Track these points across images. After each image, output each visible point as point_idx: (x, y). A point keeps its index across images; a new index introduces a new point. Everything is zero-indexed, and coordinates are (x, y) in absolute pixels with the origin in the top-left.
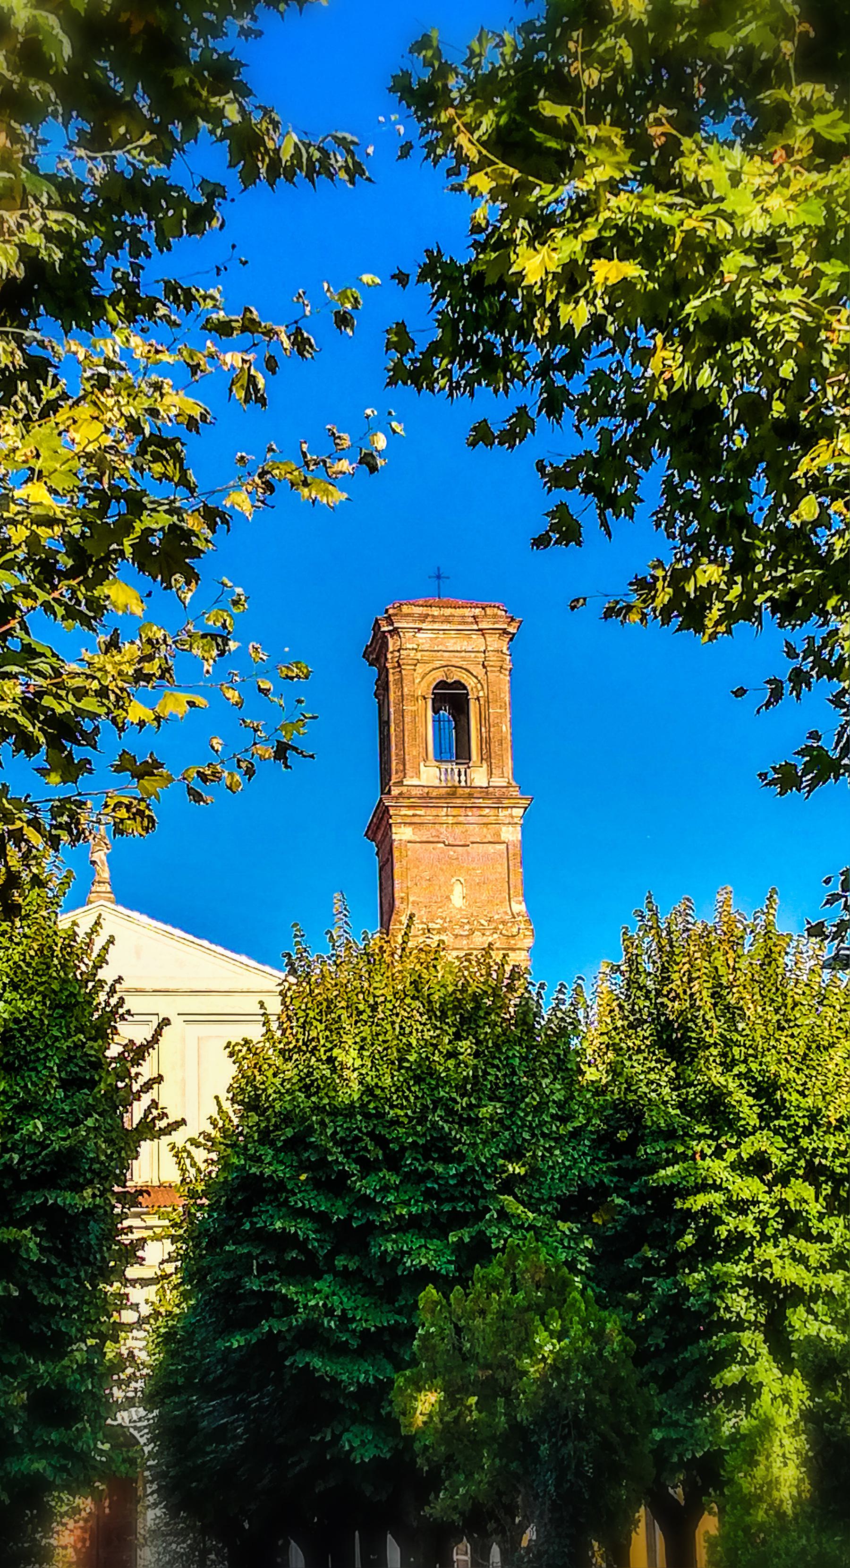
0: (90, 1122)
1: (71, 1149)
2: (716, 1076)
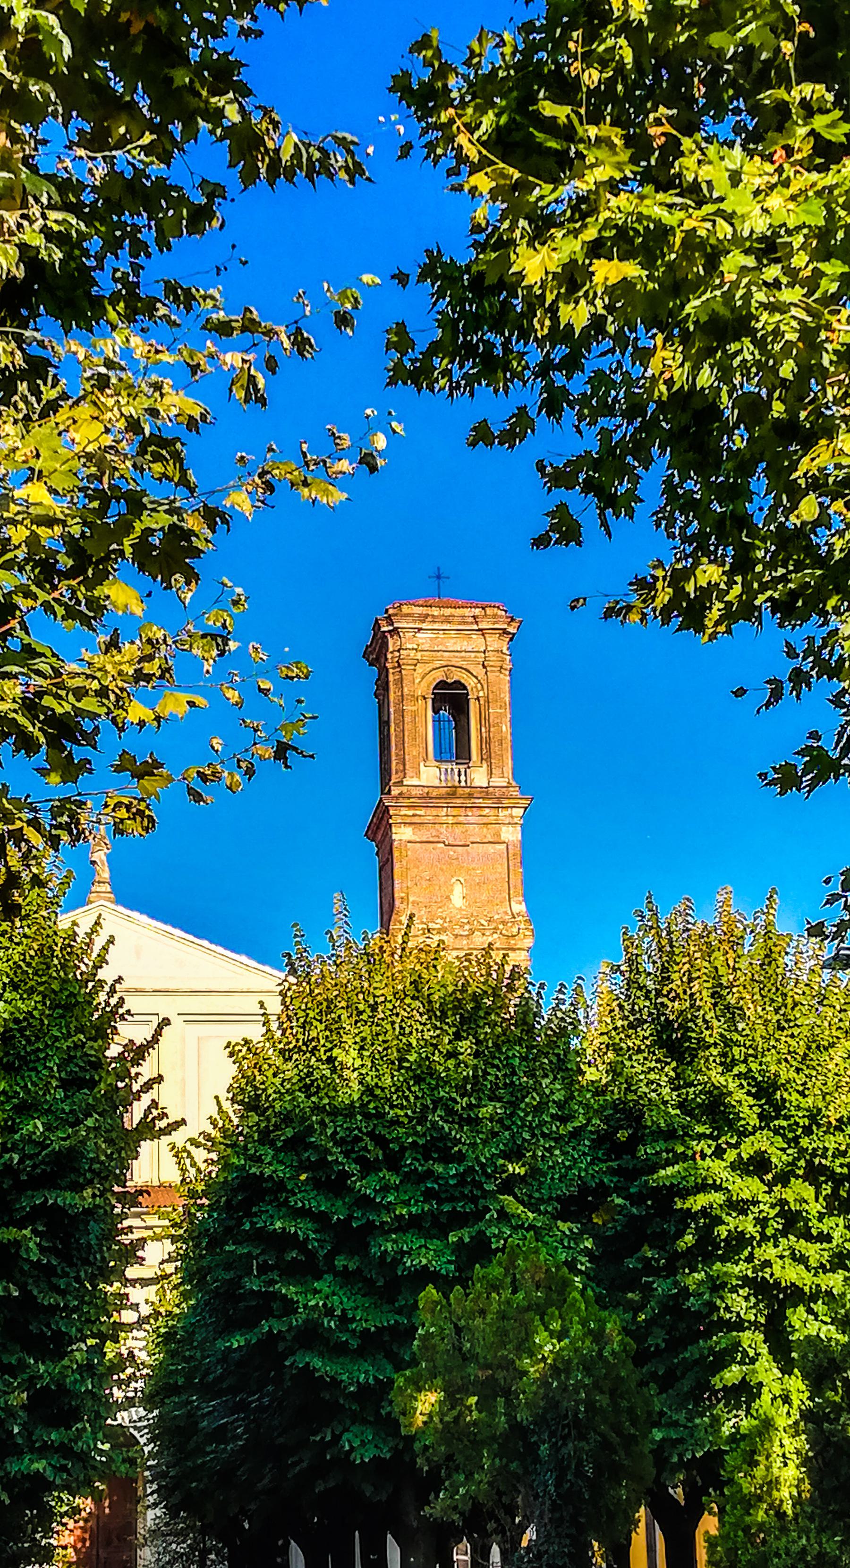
0: (90, 1122)
1: (71, 1149)
2: (716, 1076)
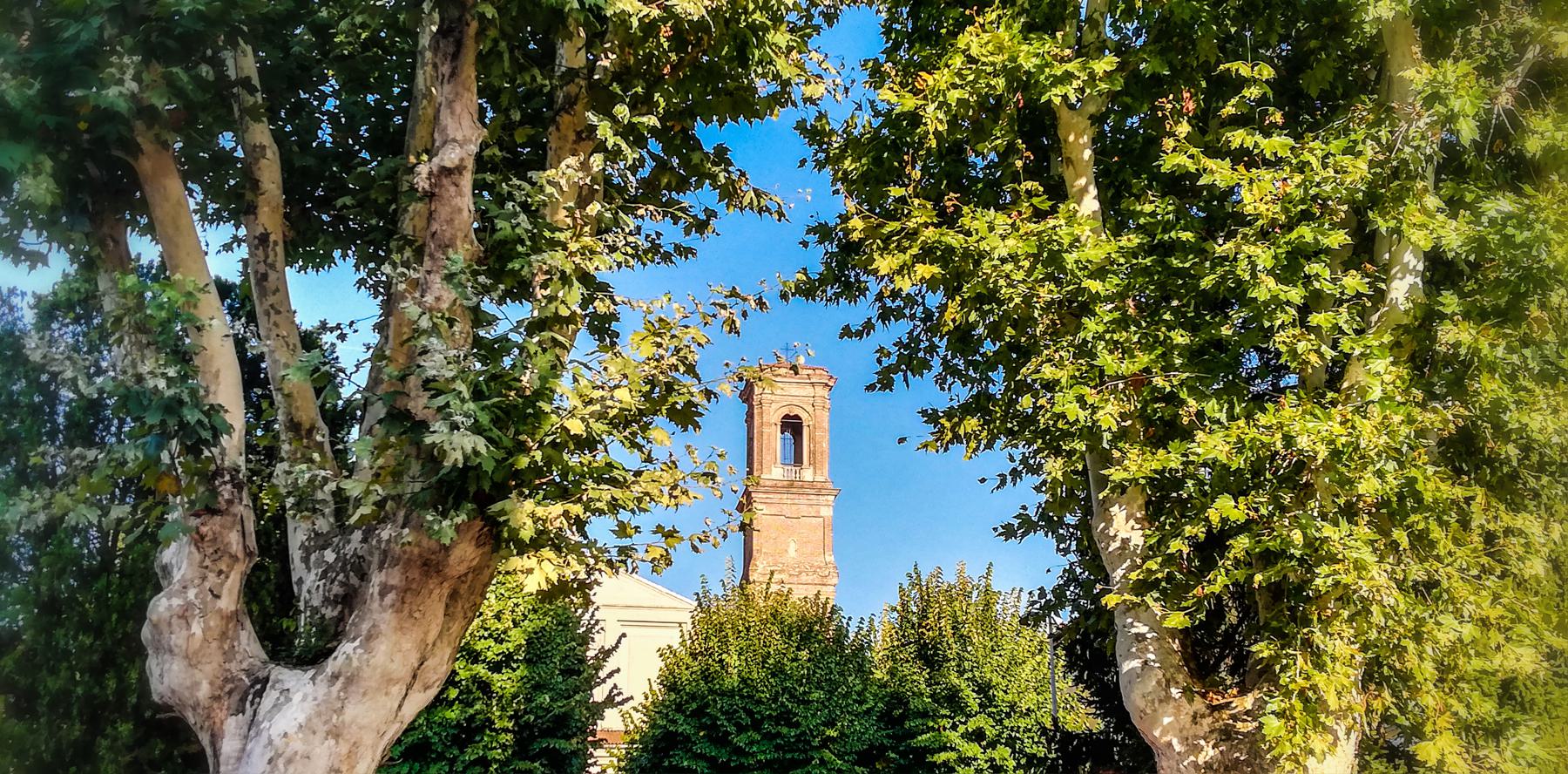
0: (577, 697)
1: (565, 714)
2: (954, 679)
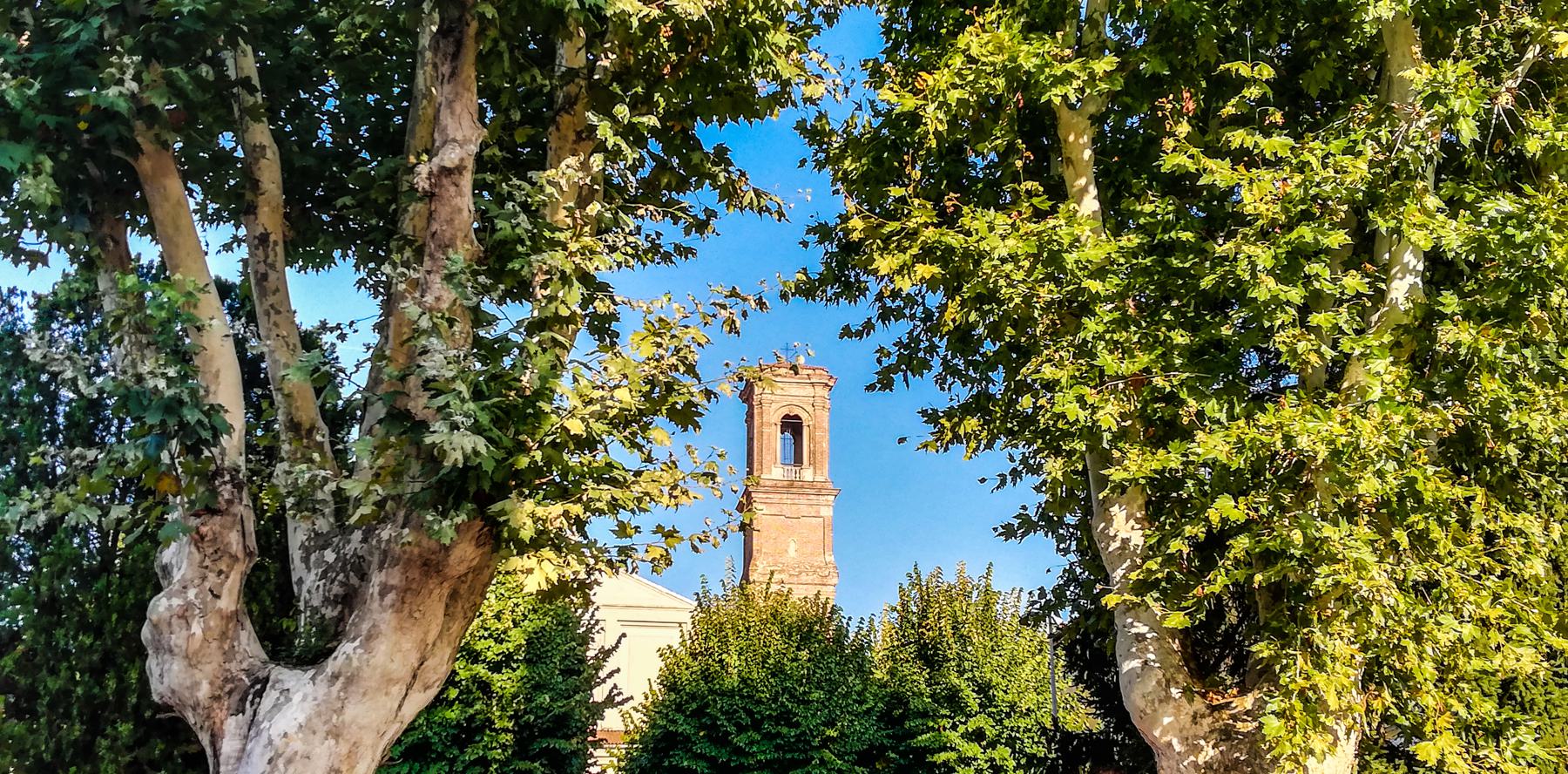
0: (577, 697)
1: (565, 714)
2: (954, 679)
